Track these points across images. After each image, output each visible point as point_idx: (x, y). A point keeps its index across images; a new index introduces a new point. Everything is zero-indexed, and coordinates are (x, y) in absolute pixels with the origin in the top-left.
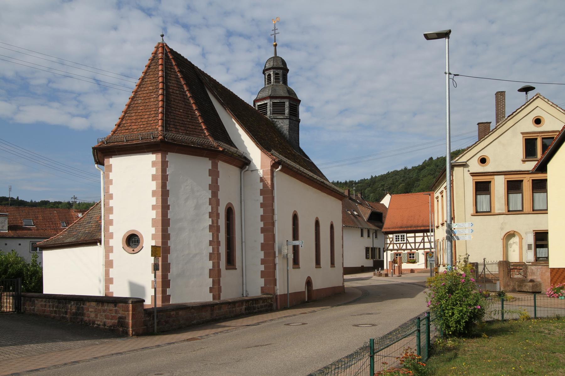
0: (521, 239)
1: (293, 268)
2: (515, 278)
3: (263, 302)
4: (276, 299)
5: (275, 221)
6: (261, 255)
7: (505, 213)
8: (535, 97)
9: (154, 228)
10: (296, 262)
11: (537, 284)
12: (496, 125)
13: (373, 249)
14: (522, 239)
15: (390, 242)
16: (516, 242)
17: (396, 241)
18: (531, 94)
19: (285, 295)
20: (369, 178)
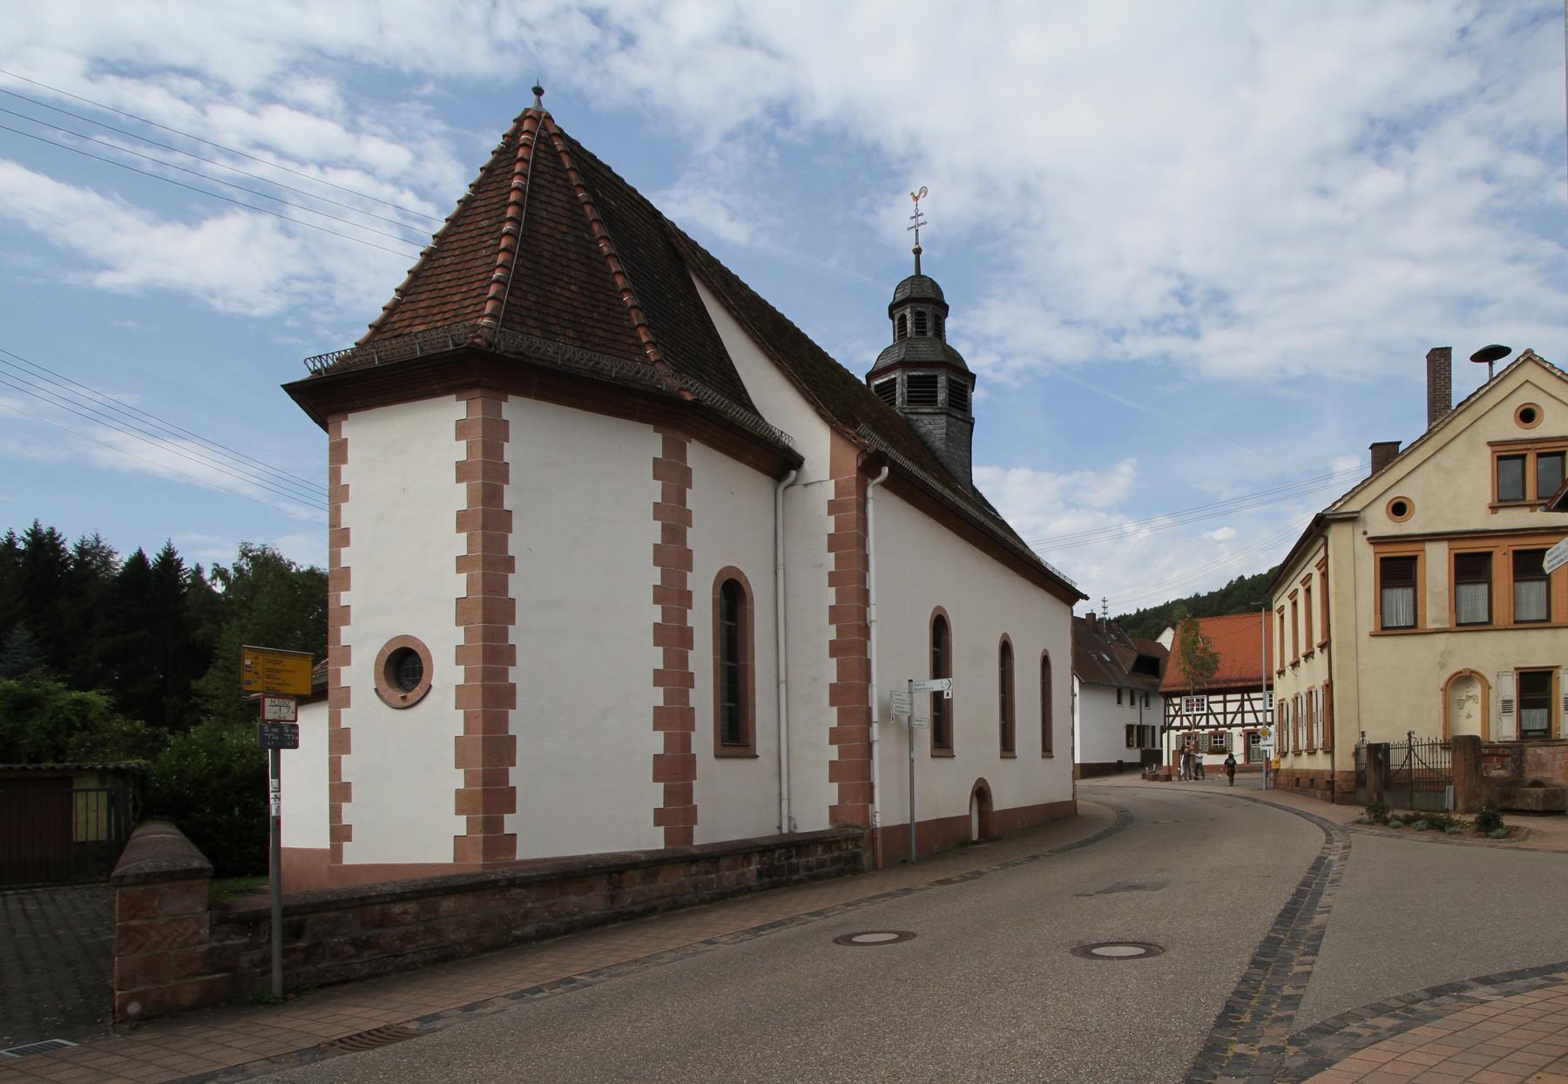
0: (1487, 688)
1: (932, 756)
2: (1494, 779)
3: (828, 849)
4: (873, 839)
5: (871, 622)
6: (831, 717)
7: (1450, 628)
8: (1522, 359)
9: (463, 628)
10: (942, 740)
11: (1555, 790)
12: (1429, 425)
13: (1142, 729)
14: (1490, 688)
15: (1174, 713)
16: (1474, 695)
17: (1187, 710)
18: (1501, 364)
19: (904, 829)
20: (1133, 612)
